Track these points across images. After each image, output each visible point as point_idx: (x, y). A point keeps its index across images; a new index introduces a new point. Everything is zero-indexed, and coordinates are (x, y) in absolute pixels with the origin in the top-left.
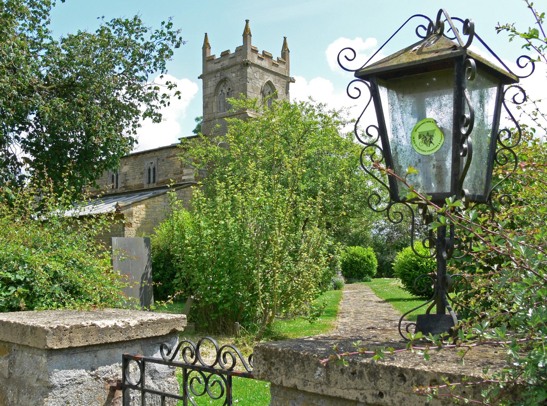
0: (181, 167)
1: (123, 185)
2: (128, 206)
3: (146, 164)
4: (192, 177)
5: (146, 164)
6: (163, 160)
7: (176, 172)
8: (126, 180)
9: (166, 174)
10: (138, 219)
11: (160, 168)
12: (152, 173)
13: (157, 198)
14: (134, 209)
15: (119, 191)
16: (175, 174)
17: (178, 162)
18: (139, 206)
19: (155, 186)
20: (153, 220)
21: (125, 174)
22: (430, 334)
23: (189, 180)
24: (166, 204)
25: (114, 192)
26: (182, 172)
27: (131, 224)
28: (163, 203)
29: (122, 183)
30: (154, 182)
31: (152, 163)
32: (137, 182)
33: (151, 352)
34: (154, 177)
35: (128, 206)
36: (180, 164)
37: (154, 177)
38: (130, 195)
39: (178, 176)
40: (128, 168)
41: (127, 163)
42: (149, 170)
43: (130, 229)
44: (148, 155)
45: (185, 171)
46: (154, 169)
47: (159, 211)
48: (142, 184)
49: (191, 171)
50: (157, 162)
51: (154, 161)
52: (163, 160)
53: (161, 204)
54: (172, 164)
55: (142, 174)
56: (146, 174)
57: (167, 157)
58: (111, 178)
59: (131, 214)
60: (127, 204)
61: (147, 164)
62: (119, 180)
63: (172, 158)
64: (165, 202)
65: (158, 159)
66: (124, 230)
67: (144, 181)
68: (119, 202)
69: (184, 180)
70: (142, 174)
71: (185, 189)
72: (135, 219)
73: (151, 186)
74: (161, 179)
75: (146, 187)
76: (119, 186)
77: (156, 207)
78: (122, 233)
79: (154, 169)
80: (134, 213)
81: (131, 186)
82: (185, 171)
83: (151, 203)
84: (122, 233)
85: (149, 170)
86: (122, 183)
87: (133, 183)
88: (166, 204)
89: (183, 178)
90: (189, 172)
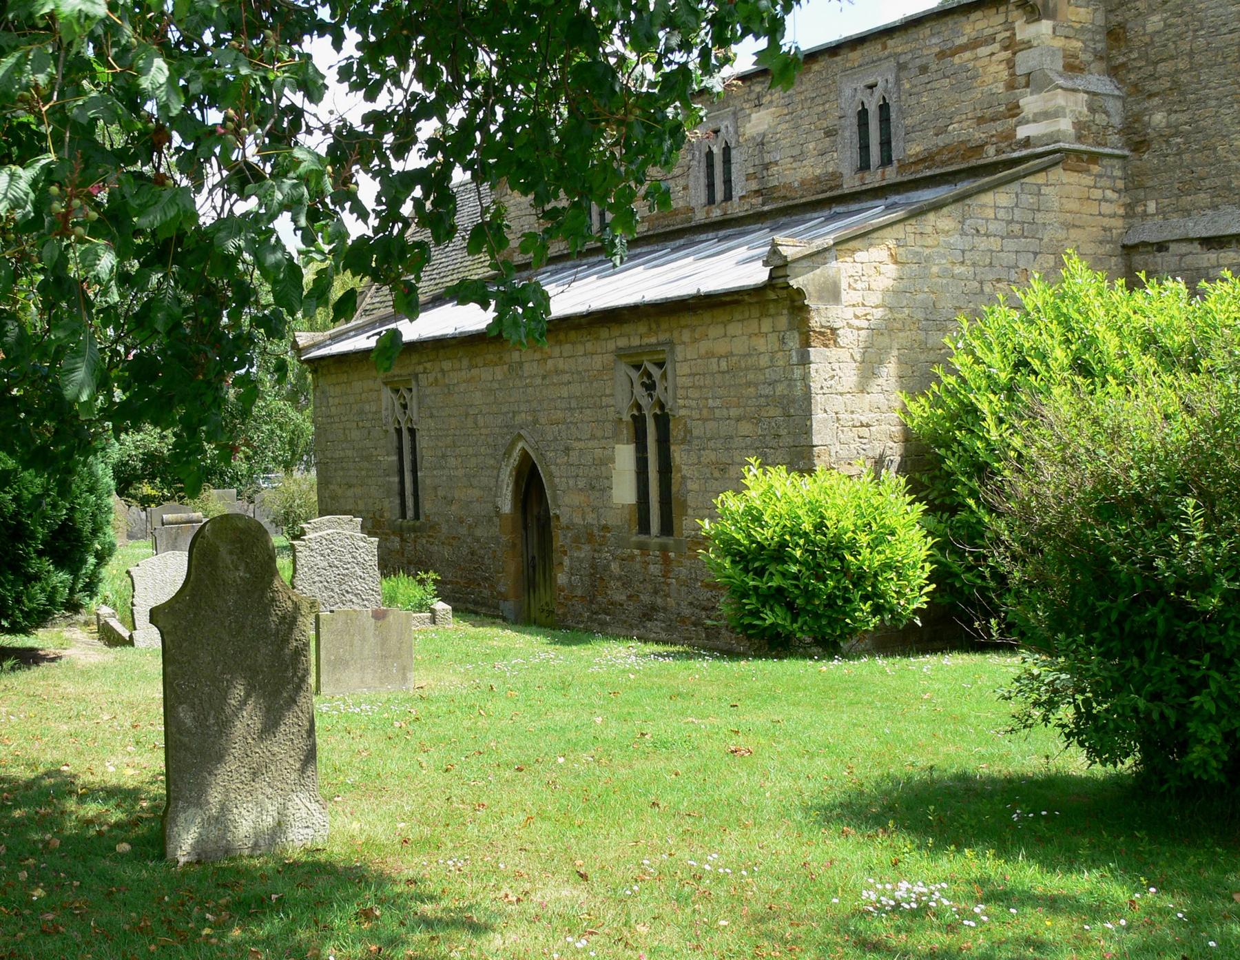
0: (1011, 86)
1: (754, 186)
2: (820, 255)
3: (848, 92)
4: (1065, 125)
5: (848, 92)
6: (924, 69)
7: (989, 113)
8: (766, 167)
9: (941, 123)
10: (860, 311)
11: (913, 101)
12: (875, 128)
13: (931, 217)
14: (842, 268)
15: (736, 208)
16: (981, 120)
17: (993, 68)
18: (860, 256)
19: (892, 175)
20: (920, 315)
21: (761, 143)
22: (925, 606)
23: (1053, 138)
24: (965, 243)
25: (716, 214)
26: (1014, 110)
27: (834, 330)
28: (955, 239)
29: (749, 177)
30: (886, 160)
31: (871, 87)
32: (811, 169)
33: (369, 525)
34: (886, 144)
35: (820, 255)
36: (1005, 75)
37: (886, 144)
38: (784, 220)
39: (999, 127)
40: (769, 119)
41: (765, 100)
42: (863, 115)
43: (833, 353)
44: (855, 56)
45: (1030, 103)
46: (884, 108)
47: (944, 273)
48: (836, 176)
49: (1060, 99)
50: (898, 80)
51: (883, 76)
52: (924, 69)
53: (949, 246)
54: (966, 80)
55: (830, 133)
56: (850, 133)
57: (942, 55)
58: (703, 165)
59: (832, 293)
60: (813, 248)
61: (851, 92)
62: (734, 169)
63: (967, 55)
64: (963, 233)
65: (901, 67)
66: (805, 360)
67: (843, 161)
68: (779, 238)
69: (1027, 142)
70: (830, 133)
71: (1040, 178)
72: (849, 313)
73: (874, 179)
74: (915, 149)
75: (851, 183)
76: (737, 192)
77: (928, 259)
78: (798, 373)
79: (884, 108)
80: (844, 285)
81: (789, 187)
82: (1030, 103)
83: (910, 240)
84: (798, 373)
85: (863, 115)
86: (749, 177)
87: (796, 171)
88: (965, 243)
89: (1022, 132)
90: (1050, 106)
